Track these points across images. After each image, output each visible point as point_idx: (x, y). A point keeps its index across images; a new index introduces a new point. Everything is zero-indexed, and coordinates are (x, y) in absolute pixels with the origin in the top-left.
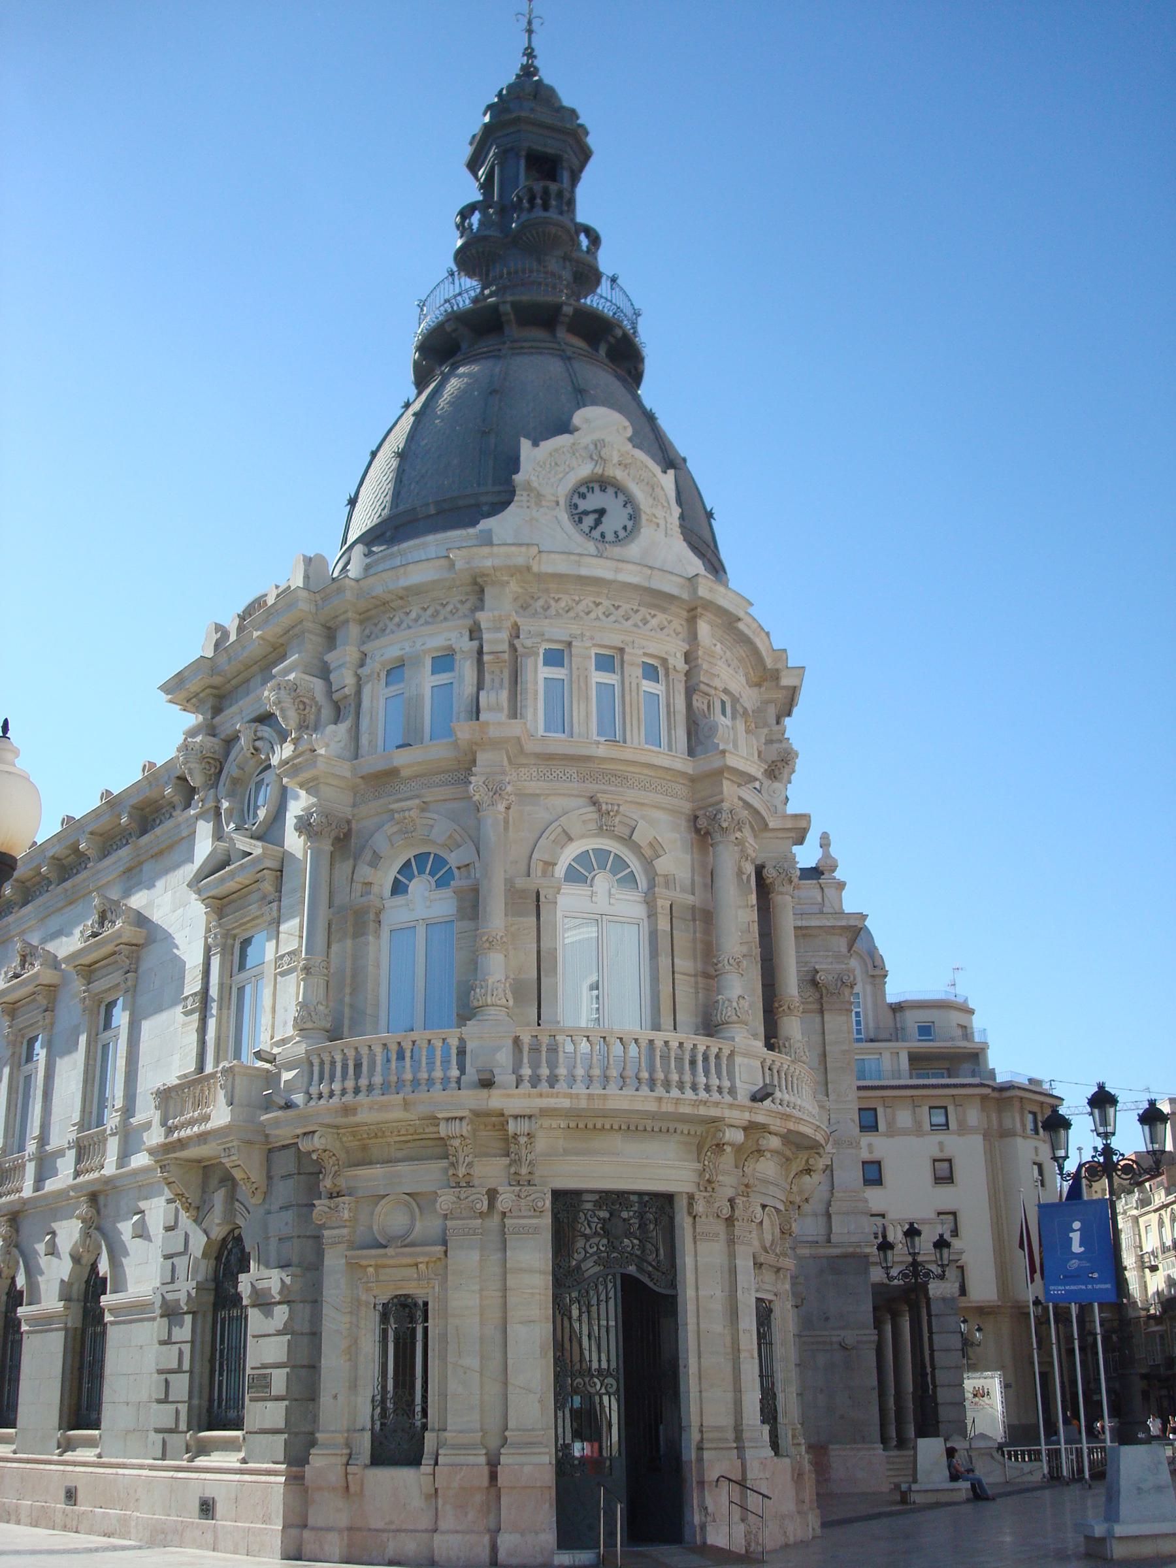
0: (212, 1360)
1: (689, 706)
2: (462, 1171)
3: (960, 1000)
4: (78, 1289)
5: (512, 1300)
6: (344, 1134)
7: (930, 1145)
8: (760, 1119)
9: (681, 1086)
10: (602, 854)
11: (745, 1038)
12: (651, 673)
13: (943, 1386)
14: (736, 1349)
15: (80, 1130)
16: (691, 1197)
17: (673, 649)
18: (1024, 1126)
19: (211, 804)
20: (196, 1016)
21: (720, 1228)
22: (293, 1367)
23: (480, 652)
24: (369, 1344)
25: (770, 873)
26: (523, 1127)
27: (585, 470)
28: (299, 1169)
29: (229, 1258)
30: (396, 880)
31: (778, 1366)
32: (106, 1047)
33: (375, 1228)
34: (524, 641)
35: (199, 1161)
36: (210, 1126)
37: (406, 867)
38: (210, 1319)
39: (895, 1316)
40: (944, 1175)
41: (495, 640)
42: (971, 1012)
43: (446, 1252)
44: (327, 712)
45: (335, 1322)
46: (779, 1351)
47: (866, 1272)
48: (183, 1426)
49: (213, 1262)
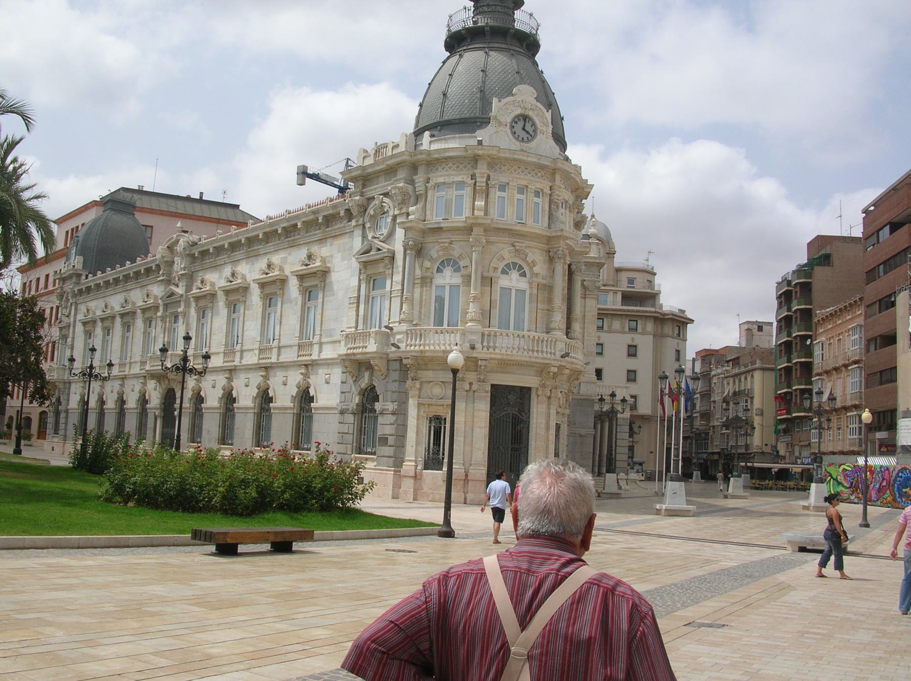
0: (361, 431)
1: (550, 207)
3: (650, 268)
7: (628, 339)
8: (564, 364)
9: (537, 351)
10: (515, 264)
11: (560, 335)
12: (537, 194)
14: (548, 440)
16: (537, 389)
17: (545, 185)
18: (673, 332)
19: (361, 222)
20: (355, 305)
21: (545, 399)
23: (475, 184)
24: (425, 430)
25: (573, 267)
26: (484, 363)
27: (519, 111)
29: (370, 395)
31: (561, 446)
34: (492, 182)
36: (367, 350)
39: (602, 422)
40: (632, 351)
41: (481, 181)
42: (655, 274)
44: (412, 200)
45: (412, 422)
46: (561, 441)
47: (593, 406)
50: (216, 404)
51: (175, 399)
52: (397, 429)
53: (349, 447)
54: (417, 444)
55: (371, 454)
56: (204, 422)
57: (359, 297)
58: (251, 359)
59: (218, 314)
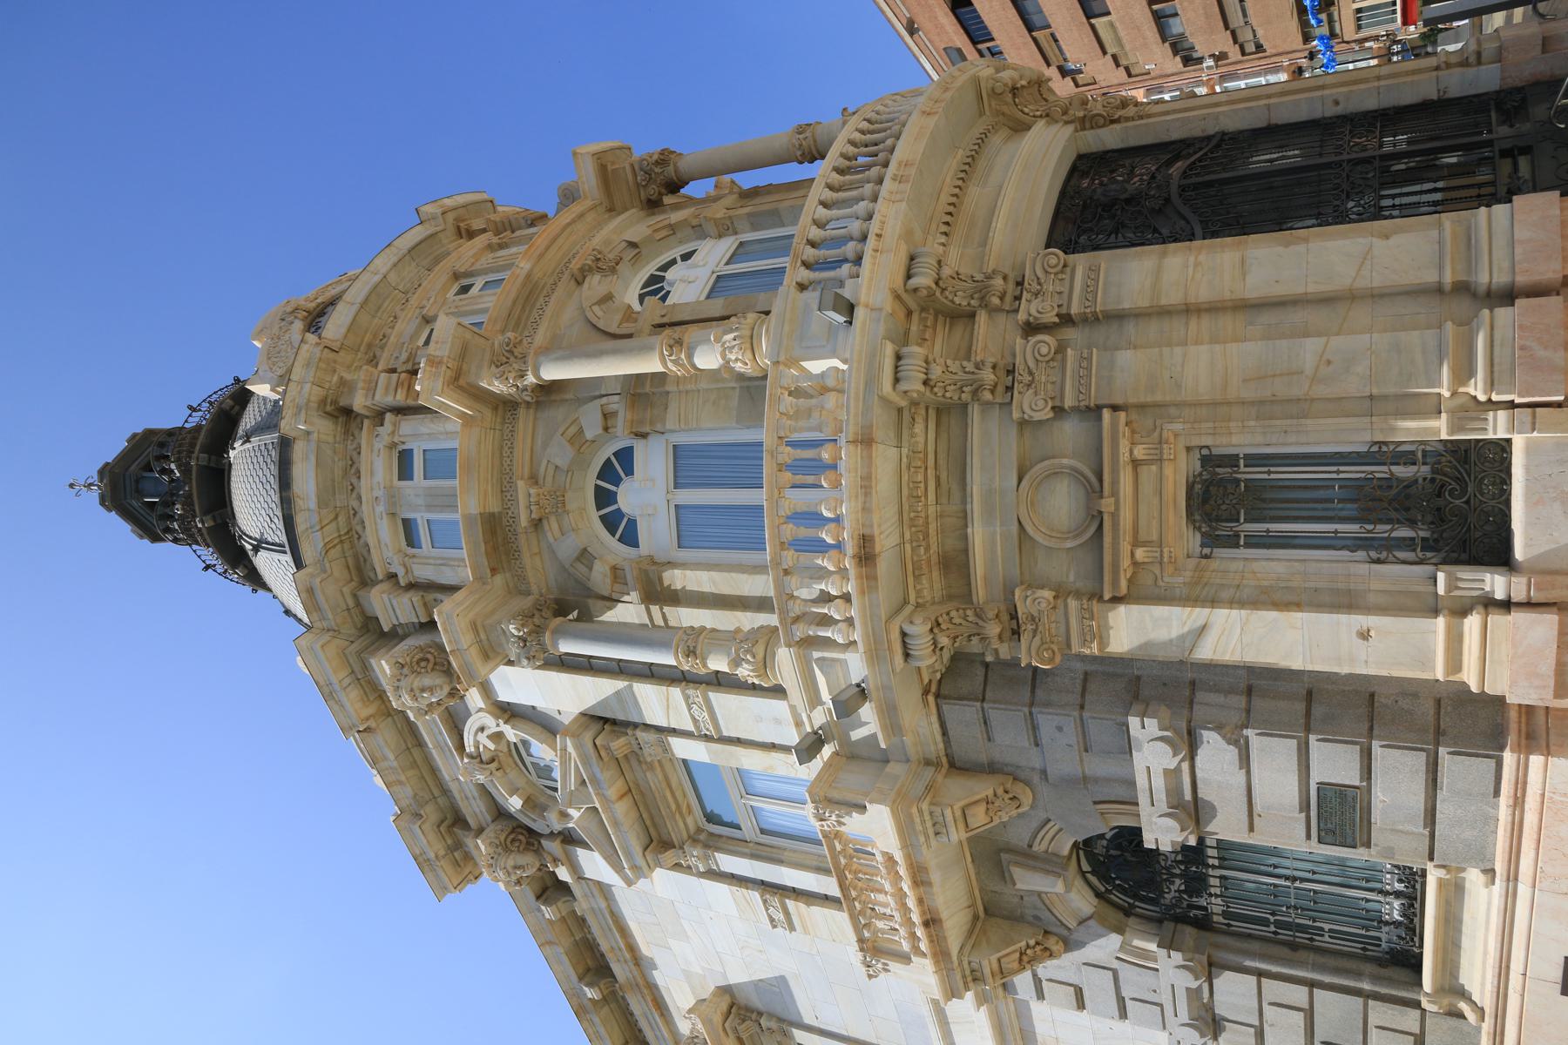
2: (988, 376)
5: (1203, 294)
6: (919, 593)
20: (790, 904)
22: (1308, 729)
28: (976, 700)
30: (602, 518)
33: (1069, 544)
35: (976, 918)
36: (898, 856)
37: (611, 523)
43: (1115, 408)
45: (1236, 636)
48: (1410, 1020)
49: (1132, 921)
51: (1389, 482)
52: (1271, 728)
53: (1380, 1013)
54: (1347, 601)
55: (1413, 899)
56: (1296, 664)
57: (765, 886)
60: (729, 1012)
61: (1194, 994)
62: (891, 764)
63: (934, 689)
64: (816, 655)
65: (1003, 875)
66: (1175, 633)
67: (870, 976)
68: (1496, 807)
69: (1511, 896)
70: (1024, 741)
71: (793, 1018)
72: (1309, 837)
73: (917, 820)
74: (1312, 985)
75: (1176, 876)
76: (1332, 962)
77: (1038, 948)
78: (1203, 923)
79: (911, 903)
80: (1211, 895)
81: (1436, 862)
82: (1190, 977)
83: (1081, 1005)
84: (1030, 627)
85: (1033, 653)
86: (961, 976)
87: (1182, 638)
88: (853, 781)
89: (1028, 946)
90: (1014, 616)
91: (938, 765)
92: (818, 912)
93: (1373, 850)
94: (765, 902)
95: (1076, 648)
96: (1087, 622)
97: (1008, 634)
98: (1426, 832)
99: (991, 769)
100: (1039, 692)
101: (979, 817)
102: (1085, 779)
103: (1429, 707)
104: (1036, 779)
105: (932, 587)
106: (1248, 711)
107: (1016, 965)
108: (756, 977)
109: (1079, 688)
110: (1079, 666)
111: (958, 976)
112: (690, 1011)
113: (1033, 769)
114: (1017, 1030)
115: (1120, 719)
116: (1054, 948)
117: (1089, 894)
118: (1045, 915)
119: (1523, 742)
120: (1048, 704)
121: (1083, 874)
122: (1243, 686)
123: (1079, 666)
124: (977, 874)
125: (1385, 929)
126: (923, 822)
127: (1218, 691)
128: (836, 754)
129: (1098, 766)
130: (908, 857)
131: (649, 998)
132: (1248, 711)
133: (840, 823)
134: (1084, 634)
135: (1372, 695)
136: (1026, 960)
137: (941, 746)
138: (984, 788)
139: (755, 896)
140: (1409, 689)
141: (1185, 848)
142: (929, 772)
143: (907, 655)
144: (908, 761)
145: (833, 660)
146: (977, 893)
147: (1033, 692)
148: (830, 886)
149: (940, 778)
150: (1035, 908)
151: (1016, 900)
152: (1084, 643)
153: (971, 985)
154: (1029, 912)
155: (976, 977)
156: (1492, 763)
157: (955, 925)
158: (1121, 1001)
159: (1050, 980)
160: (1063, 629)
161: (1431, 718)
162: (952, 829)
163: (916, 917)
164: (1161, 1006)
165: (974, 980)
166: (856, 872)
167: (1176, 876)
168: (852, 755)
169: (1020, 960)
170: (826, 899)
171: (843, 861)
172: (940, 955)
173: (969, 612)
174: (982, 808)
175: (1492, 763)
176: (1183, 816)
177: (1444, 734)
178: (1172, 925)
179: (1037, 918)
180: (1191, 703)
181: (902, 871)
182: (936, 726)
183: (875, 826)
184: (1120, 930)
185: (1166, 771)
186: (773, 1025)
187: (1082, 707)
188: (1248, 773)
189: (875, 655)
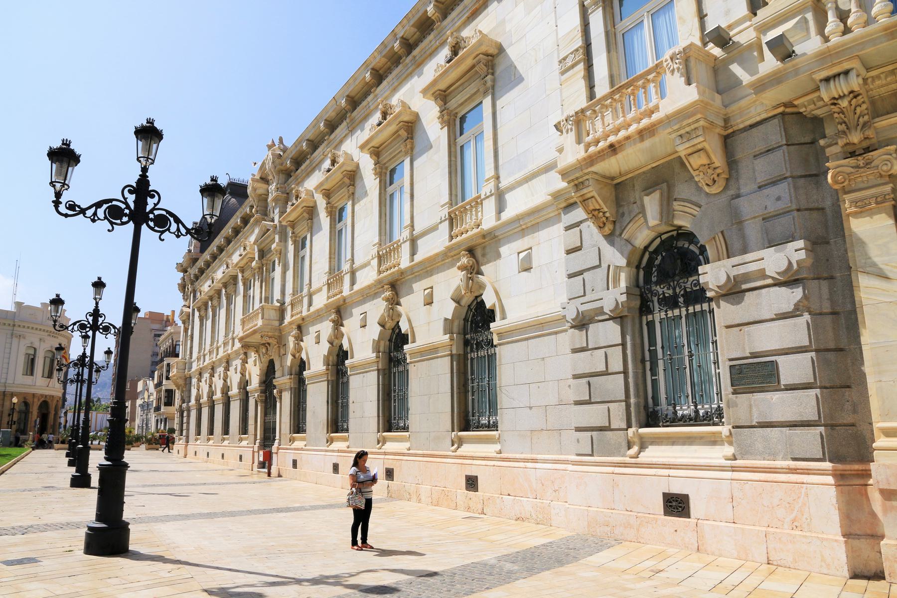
4: (333, 359)
6: (878, 77)
13: (621, 401)
15: (449, 208)
20: (581, 66)
32: (340, 231)
35: (613, 178)
36: (655, 117)
38: (637, 321)
49: (634, 270)
50: (439, 337)
52: (814, 329)
53: (618, 410)
56: (866, 338)
58: (434, 244)
59: (320, 229)
60: (488, 56)
61: (600, 310)
62: (719, 97)
63: (788, 110)
64: (809, 16)
65: (648, 189)
66: (877, 260)
67: (557, 127)
68: (784, 459)
69: (722, 469)
70: (761, 179)
71: (497, 94)
72: (731, 360)
73: (691, 120)
74: (625, 372)
75: (674, 289)
76: (640, 382)
77: (604, 219)
78: (645, 308)
79: (622, 134)
80: (666, 311)
81: (733, 430)
82: (612, 307)
83: (569, 252)
84: (861, 163)
85: (838, 170)
86: (577, 177)
87: (874, 265)
88: (701, 71)
89: (604, 213)
90: (868, 150)
91: (726, 128)
92: (581, 85)
93: (731, 396)
94: (577, 50)
95: (847, 198)
96: (873, 201)
97: (850, 149)
98: (754, 423)
99: (732, 162)
100: (803, 180)
101: (697, 161)
102: (740, 223)
103: (849, 419)
104: (731, 192)
105: (882, 86)
106: (820, 314)
107: (591, 208)
108: (516, 63)
109: (812, 206)
110: (828, 203)
111: (577, 175)
112: (480, 32)
113: (739, 189)
114: (538, 221)
115: (797, 235)
116: (606, 229)
117: (646, 243)
118: (627, 219)
119: (838, 472)
120: (796, 188)
121: (660, 235)
122: (838, 309)
123: (828, 203)
124: (644, 173)
125: (671, 408)
126: (689, 125)
127: (831, 294)
128: (716, 58)
129: (753, 230)
130: (660, 122)
131: (477, 6)
132: (820, 314)
133: (673, 72)
134: (862, 200)
135: (849, 387)
136: (594, 214)
137: (741, 126)
138: (718, 160)
139: (579, 42)
140: (862, 405)
141: (703, 291)
142: (722, 123)
143: (827, 80)
144: (726, 106)
145: (808, 29)
146: (631, 175)
147: (801, 177)
148: (602, 88)
149: (718, 130)
150: (630, 212)
151: (632, 200)
152: (854, 202)
153: (572, 184)
154: (625, 210)
155: (578, 185)
156: (820, 455)
157: (611, 166)
158: (580, 273)
159: (581, 232)
160: (862, 186)
161: (841, 421)
162: (687, 145)
163: (612, 139)
164: (584, 295)
165: (576, 185)
166: (633, 94)
167: (674, 289)
168: (718, 69)
169: (595, 210)
170: (591, 87)
171: (640, 83)
172: (591, 160)
173: (866, 118)
174: (705, 161)
175: (820, 455)
176: (730, 286)
177: (832, 429)
178: (639, 293)
179: (623, 214)
180: (818, 279)
181: (645, 122)
182: (758, 119)
183: (679, 94)
184: (628, 264)
185: (602, 307)
186: (489, 83)
187: (798, 210)
188: (773, 320)
189: (823, 57)
